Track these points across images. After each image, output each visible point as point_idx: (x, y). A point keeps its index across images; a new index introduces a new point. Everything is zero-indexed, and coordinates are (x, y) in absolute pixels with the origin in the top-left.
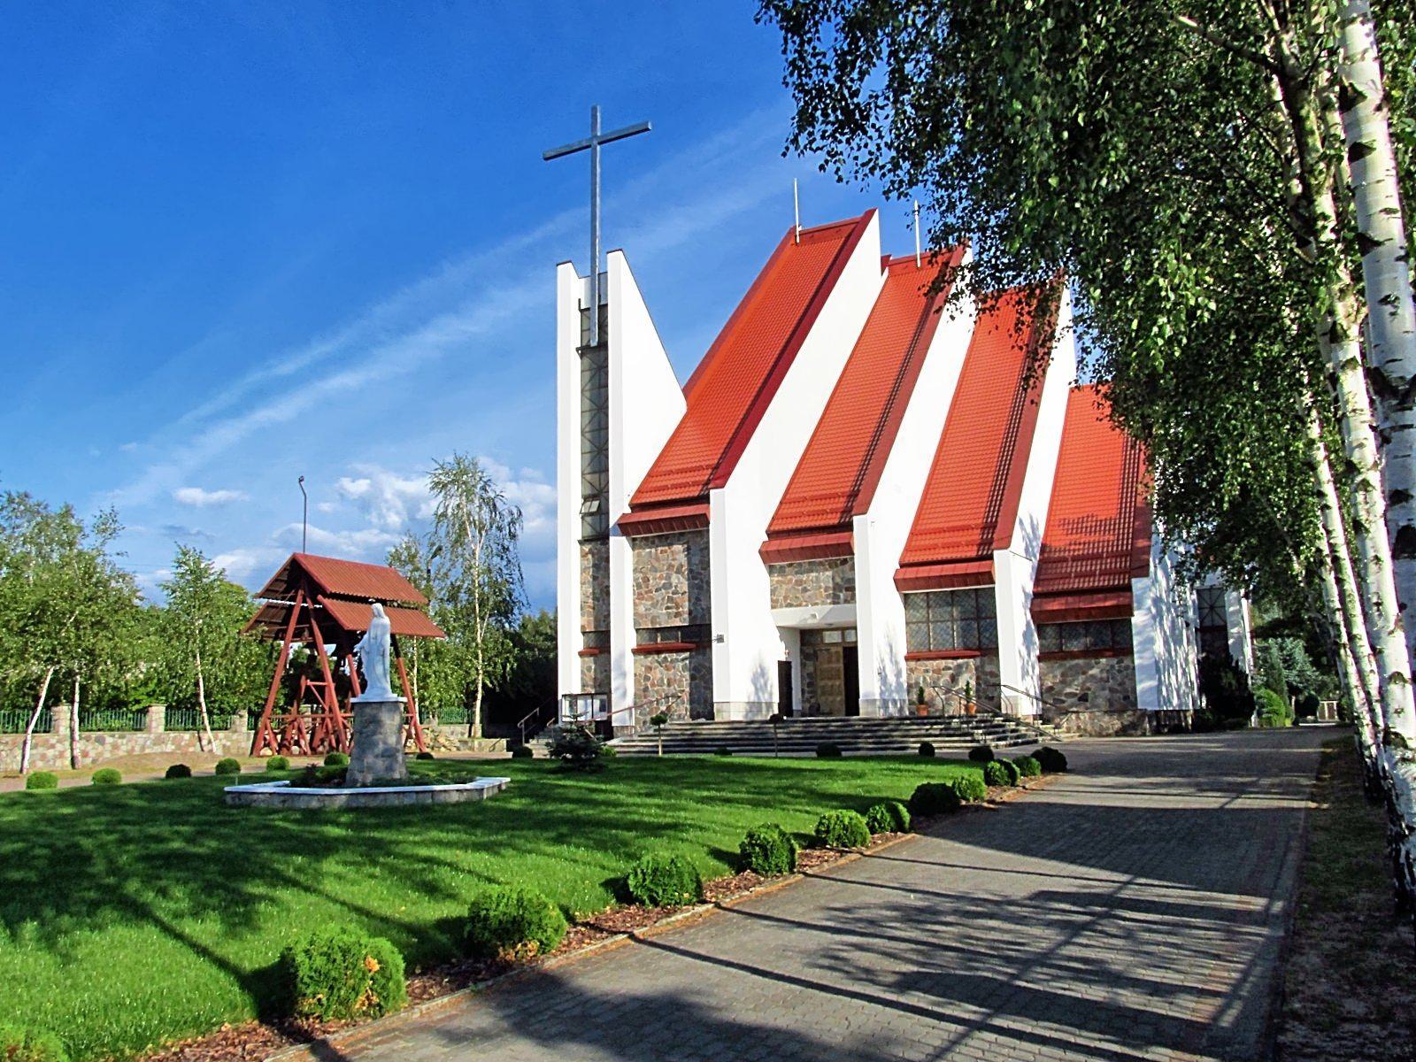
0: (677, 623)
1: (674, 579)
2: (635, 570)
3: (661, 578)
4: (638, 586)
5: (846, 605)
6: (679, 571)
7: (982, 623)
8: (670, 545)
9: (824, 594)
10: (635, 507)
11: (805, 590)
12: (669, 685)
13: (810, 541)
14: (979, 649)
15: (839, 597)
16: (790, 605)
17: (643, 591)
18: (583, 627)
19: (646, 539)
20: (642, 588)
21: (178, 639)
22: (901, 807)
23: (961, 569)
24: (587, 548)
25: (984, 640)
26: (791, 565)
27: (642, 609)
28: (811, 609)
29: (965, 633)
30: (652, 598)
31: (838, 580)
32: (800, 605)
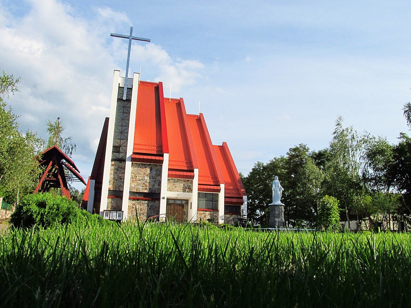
0: (146, 191)
1: (146, 178)
2: (132, 173)
3: (141, 177)
4: (132, 178)
5: (188, 193)
6: (147, 176)
7: (213, 202)
8: (146, 167)
9: (181, 189)
10: (134, 153)
11: (176, 187)
12: (141, 210)
13: (178, 173)
14: (212, 209)
15: (186, 190)
16: (171, 191)
17: (134, 180)
18: (109, 188)
19: (137, 164)
20: (134, 179)
21: (274, 169)
22: (80, 253)
23: (209, 187)
24: (113, 163)
25: (213, 207)
26: (172, 179)
27: (133, 185)
28: (177, 193)
29: (207, 205)
30: (137, 183)
31: (186, 185)
32: (174, 191)
